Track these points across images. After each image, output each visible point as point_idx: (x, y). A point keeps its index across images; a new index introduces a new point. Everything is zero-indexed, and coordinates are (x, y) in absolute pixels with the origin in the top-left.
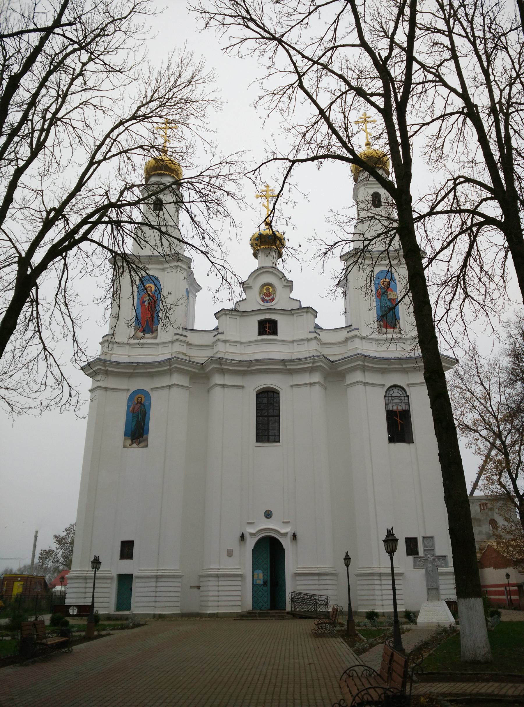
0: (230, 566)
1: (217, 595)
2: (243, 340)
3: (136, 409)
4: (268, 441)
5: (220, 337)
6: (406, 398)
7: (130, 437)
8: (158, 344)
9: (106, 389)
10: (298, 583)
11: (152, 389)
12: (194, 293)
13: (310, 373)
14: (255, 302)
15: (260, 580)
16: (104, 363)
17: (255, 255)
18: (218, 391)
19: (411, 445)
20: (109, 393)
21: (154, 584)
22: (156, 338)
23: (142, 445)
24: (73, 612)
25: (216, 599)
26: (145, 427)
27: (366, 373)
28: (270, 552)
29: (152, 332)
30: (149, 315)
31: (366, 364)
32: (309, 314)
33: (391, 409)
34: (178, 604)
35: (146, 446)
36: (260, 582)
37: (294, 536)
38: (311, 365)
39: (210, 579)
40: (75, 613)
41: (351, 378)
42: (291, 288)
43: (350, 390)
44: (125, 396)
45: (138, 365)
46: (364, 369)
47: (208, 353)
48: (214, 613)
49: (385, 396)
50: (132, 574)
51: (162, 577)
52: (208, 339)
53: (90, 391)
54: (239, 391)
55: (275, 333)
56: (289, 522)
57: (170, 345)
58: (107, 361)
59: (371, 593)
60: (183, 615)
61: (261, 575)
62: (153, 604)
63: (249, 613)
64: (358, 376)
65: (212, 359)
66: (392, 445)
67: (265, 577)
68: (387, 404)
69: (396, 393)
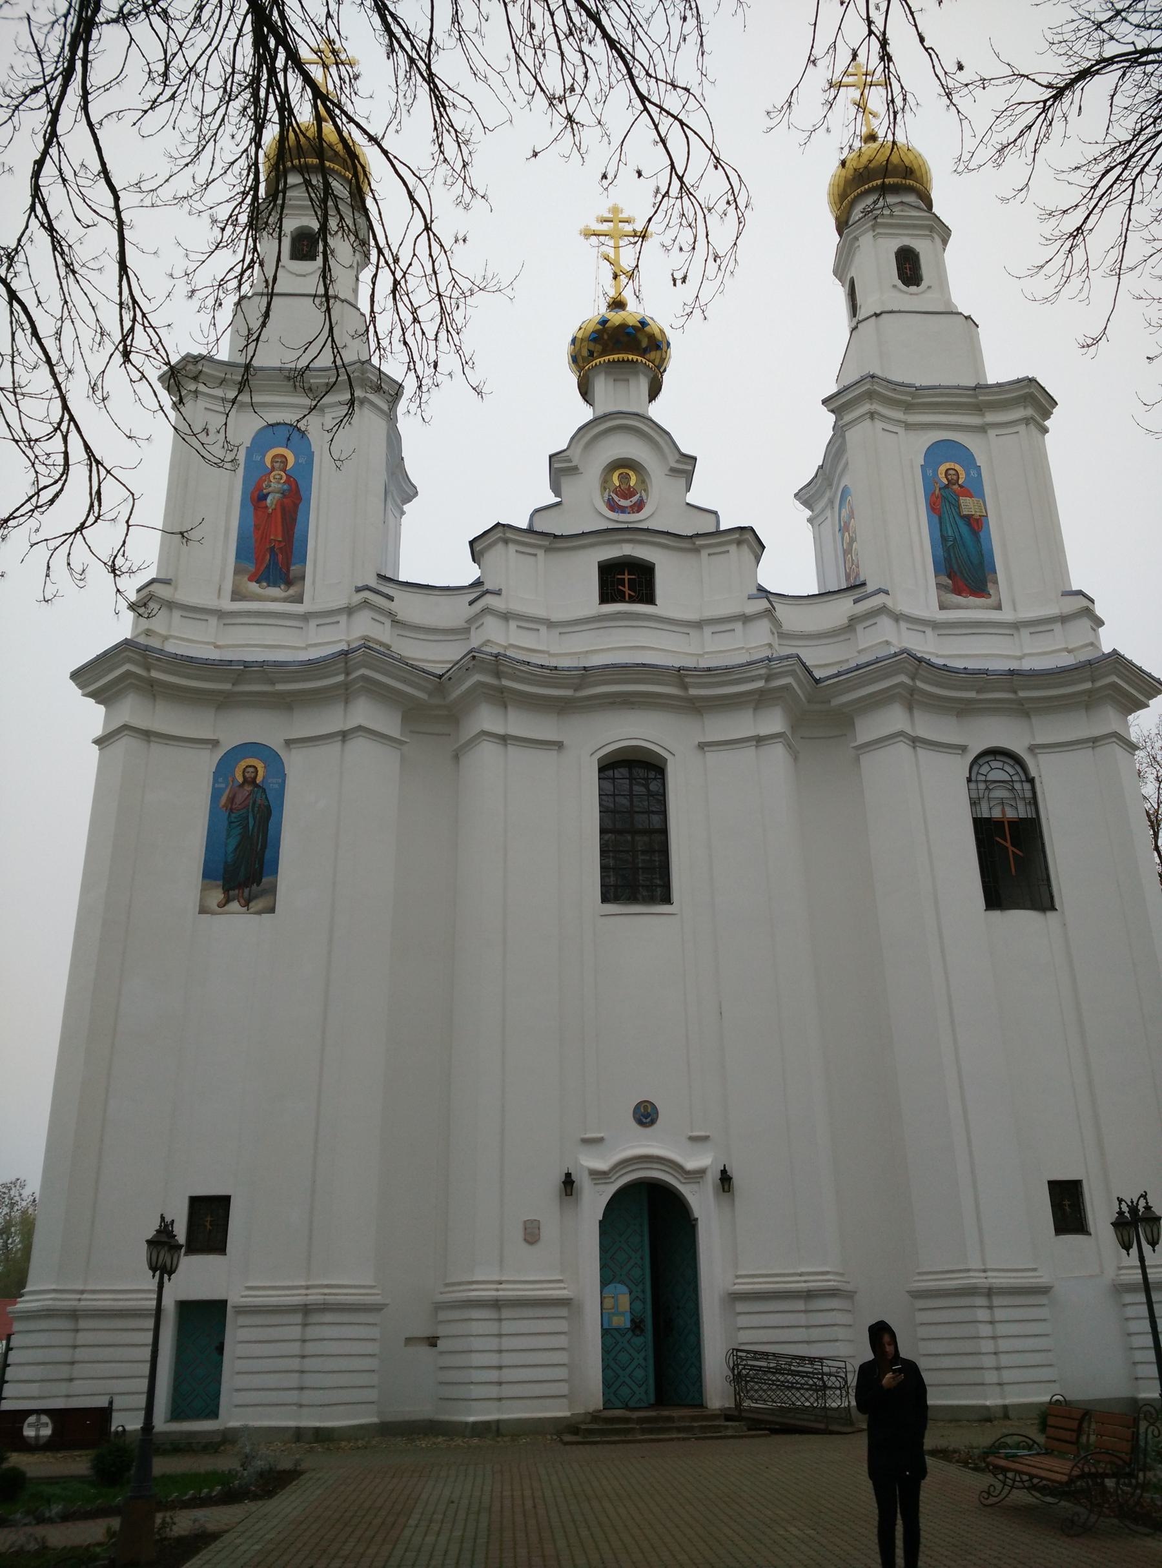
0: (530, 1272)
1: (495, 1363)
2: (555, 617)
3: (239, 799)
4: (633, 899)
5: (489, 600)
6: (1027, 786)
7: (220, 883)
8: (306, 617)
9: (147, 735)
10: (742, 1321)
11: (289, 743)
12: (399, 502)
13: (755, 709)
14: (588, 510)
15: (623, 1314)
16: (145, 657)
17: (585, 390)
18: (488, 751)
19: (1050, 915)
20: (157, 750)
21: (296, 1332)
22: (299, 599)
23: (256, 905)
24: (37, 1430)
25: (493, 1375)
26: (268, 855)
27: (916, 713)
28: (652, 1226)
29: (289, 583)
30: (273, 545)
31: (919, 684)
32: (745, 548)
33: (986, 815)
34: (373, 1395)
35: (272, 910)
36: (623, 1321)
37: (725, 1179)
38: (760, 684)
39: (476, 1314)
40: (47, 1432)
41: (869, 728)
42: (688, 476)
43: (866, 760)
44: (208, 761)
45: (246, 670)
46: (912, 700)
47: (453, 652)
48: (488, 1423)
49: (969, 780)
50: (223, 1303)
51: (325, 1308)
52: (456, 612)
53: (97, 742)
54: (548, 757)
55: (650, 599)
56: (706, 1139)
57: (343, 619)
58: (153, 650)
59: (968, 1346)
60: (388, 1430)
61: (625, 1300)
62: (293, 1396)
63: (595, 1417)
64: (894, 719)
65: (473, 655)
66: (996, 915)
67: (638, 1305)
68: (974, 803)
69: (998, 772)
